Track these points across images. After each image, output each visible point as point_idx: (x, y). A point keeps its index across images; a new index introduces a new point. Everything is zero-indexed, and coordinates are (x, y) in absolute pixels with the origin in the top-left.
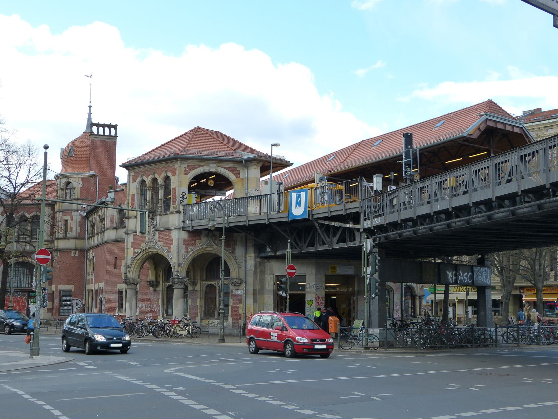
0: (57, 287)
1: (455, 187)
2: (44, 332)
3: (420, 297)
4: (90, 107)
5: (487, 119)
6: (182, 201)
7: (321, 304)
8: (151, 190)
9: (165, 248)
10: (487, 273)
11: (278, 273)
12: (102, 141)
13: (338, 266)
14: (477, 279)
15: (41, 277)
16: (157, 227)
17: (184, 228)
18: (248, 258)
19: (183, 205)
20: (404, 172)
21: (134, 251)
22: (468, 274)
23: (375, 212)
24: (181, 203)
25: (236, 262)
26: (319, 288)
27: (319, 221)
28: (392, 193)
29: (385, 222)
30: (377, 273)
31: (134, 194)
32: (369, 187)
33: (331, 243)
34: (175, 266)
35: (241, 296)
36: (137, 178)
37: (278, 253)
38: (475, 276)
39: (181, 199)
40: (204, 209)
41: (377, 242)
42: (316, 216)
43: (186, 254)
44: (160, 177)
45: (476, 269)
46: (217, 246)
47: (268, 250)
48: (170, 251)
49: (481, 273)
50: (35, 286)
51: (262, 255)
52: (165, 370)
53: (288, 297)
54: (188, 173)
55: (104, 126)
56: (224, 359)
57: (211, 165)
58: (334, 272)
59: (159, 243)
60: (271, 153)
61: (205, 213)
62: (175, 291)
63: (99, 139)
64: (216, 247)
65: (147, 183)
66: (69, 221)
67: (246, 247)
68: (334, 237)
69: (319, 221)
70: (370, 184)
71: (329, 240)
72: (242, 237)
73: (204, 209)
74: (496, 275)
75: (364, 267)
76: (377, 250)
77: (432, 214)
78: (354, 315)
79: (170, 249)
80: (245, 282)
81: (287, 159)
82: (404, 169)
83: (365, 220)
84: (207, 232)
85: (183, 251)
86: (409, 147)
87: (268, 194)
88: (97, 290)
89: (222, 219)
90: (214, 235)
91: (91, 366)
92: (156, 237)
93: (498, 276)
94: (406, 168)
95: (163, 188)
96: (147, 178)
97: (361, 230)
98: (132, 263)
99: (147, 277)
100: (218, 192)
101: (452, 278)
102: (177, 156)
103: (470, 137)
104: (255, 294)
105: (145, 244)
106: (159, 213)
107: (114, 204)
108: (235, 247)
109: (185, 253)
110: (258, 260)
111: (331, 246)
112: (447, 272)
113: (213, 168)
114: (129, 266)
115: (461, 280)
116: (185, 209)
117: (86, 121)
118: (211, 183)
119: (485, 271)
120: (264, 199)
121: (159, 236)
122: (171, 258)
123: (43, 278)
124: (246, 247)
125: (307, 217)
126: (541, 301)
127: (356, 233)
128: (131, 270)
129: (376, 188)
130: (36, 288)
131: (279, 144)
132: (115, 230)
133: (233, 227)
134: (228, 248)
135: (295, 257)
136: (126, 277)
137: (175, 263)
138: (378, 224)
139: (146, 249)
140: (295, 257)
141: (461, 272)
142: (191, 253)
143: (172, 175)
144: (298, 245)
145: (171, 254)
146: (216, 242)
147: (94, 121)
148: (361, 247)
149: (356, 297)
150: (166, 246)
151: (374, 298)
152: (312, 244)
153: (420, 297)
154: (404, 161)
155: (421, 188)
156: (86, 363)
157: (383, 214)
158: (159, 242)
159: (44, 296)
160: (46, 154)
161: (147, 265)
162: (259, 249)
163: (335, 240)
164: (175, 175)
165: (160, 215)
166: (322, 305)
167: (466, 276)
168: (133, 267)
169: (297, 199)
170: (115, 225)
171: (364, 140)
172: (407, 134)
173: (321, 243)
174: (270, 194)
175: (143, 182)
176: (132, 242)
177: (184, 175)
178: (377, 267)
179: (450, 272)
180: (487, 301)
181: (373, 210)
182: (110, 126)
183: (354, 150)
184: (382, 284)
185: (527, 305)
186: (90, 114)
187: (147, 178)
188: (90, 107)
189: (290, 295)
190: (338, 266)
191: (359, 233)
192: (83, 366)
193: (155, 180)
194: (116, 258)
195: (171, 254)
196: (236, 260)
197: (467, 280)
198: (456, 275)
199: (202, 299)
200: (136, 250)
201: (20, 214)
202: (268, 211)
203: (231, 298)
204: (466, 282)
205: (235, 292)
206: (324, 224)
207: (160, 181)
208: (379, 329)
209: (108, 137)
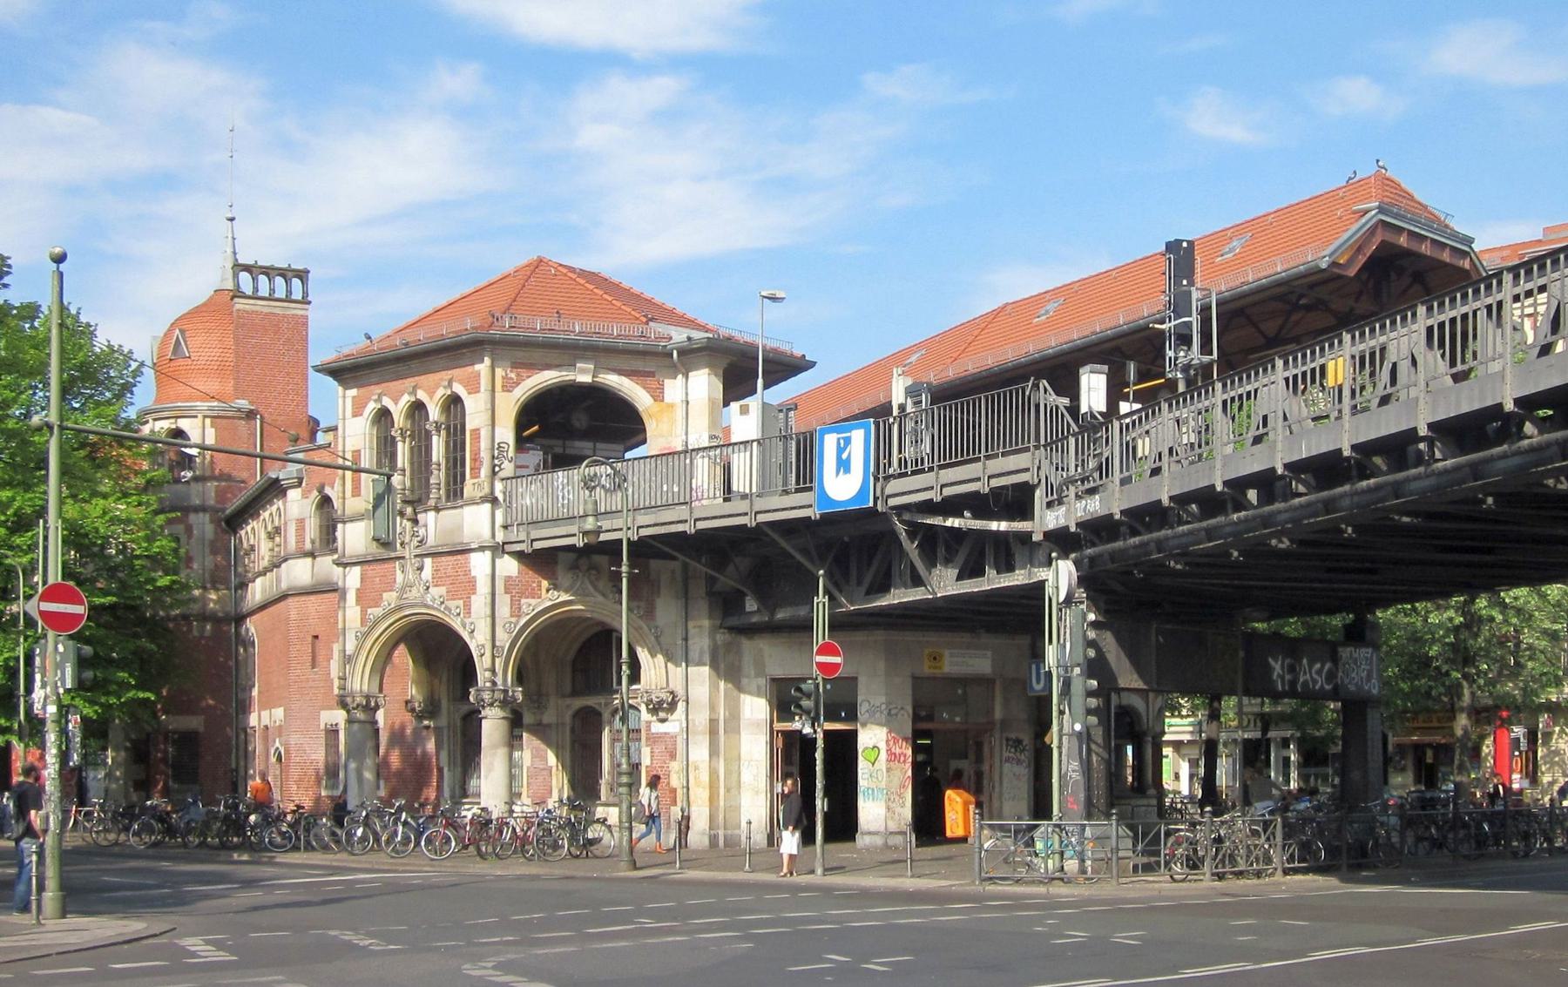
2: (1109, 838)
6: (500, 466)
7: (902, 759)
8: (407, 439)
9: (452, 604)
10: (1371, 663)
11: (779, 673)
12: (267, 314)
13: (947, 653)
14: (1346, 681)
15: (59, 672)
16: (428, 545)
18: (692, 631)
19: (503, 479)
20: (1170, 358)
21: (364, 612)
22: (1323, 666)
25: (659, 644)
26: (896, 715)
27: (907, 517)
28: (1134, 422)
31: (359, 451)
32: (1062, 408)
35: (674, 737)
36: (366, 404)
37: (781, 615)
38: (1340, 674)
40: (563, 489)
42: (893, 502)
43: (514, 620)
44: (431, 398)
45: (1345, 652)
46: (604, 595)
47: (751, 605)
48: (468, 612)
49: (1356, 664)
50: (42, 700)
52: (465, 966)
53: (820, 736)
54: (514, 388)
55: (269, 271)
56: (649, 923)
58: (936, 668)
59: (434, 591)
61: (566, 502)
62: (487, 726)
64: (600, 598)
65: (396, 417)
67: (687, 599)
69: (907, 517)
72: (673, 572)
73: (563, 489)
76: (1085, 595)
78: (993, 787)
79: (468, 607)
80: (684, 698)
81: (798, 352)
82: (1170, 349)
83: (1049, 505)
84: (572, 556)
85: (504, 610)
86: (1185, 282)
87: (753, 441)
88: (266, 727)
90: (593, 567)
91: (221, 953)
92: (427, 573)
95: (443, 433)
96: (396, 404)
98: (359, 649)
99: (405, 690)
100: (600, 445)
101: (1282, 678)
102: (480, 335)
103: (1336, 270)
104: (713, 731)
105: (394, 594)
106: (432, 503)
107: (304, 484)
108: (653, 600)
109: (512, 616)
110: (721, 637)
112: (1270, 660)
114: (350, 656)
115: (1305, 683)
116: (509, 489)
119: (1367, 658)
120: (742, 454)
121: (436, 571)
122: (473, 631)
123: (63, 674)
124: (687, 599)
125: (871, 504)
128: (356, 670)
129: (1090, 407)
130: (44, 707)
132: (309, 560)
133: (651, 541)
134: (635, 604)
135: (838, 625)
136: (342, 688)
137: (483, 646)
138: (1095, 516)
139: (400, 608)
141: (1305, 661)
142: (528, 617)
143: (469, 393)
145: (470, 620)
146: (601, 584)
150: (454, 599)
154: (1169, 325)
156: (208, 942)
158: (436, 586)
161: (402, 655)
162: (726, 606)
164: (475, 393)
165: (437, 509)
166: (904, 761)
167: (1319, 672)
168: (362, 658)
169: (840, 451)
170: (308, 546)
171: (1007, 304)
174: (758, 441)
175: (383, 415)
176: (358, 590)
177: (503, 391)
179: (1276, 662)
180: (1369, 743)
182: (285, 273)
183: (983, 330)
185: (1397, 758)
187: (396, 401)
189: (827, 733)
190: (947, 653)
192: (194, 955)
193: (418, 408)
194: (316, 637)
195: (470, 620)
197: (1321, 683)
198: (1292, 669)
199: (563, 747)
200: (369, 611)
203: (647, 746)
204: (1317, 687)
205: (658, 728)
207: (434, 413)
209: (286, 304)
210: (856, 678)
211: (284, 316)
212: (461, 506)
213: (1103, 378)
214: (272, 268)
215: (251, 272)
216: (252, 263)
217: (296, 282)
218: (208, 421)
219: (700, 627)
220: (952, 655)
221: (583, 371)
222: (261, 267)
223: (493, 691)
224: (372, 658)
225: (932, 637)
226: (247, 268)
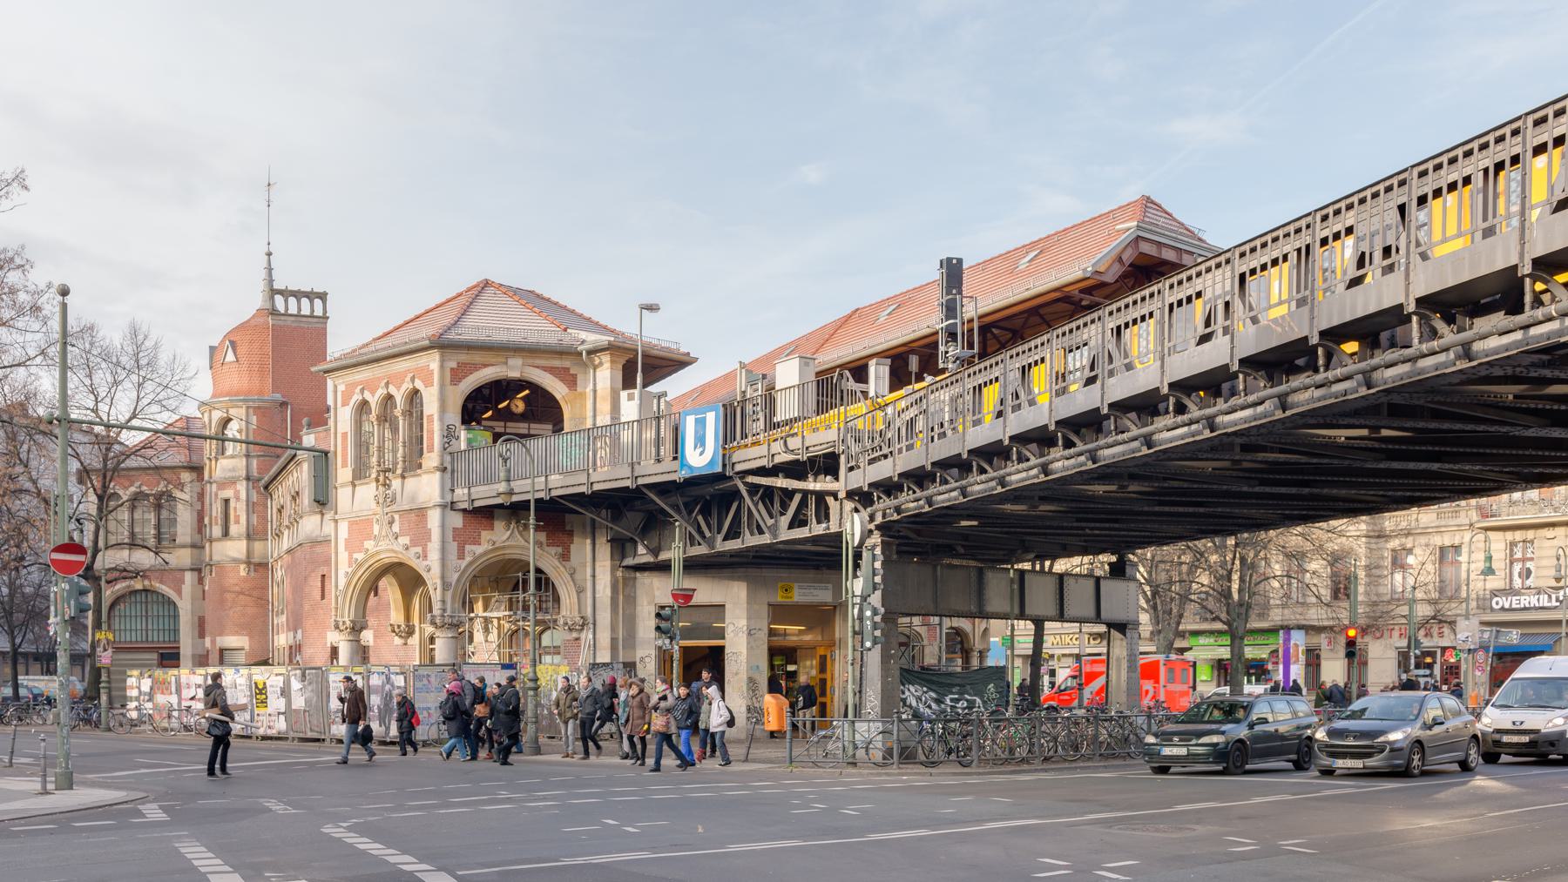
0: (213, 642)
1: (1063, 375)
3: (980, 652)
4: (269, 254)
5: (1138, 237)
12: (295, 328)
17: (452, 505)
23: (873, 449)
24: (445, 449)
25: (573, 580)
27: (751, 479)
29: (894, 471)
30: (878, 593)
33: (774, 530)
34: (435, 589)
39: (446, 440)
41: (879, 519)
42: (739, 468)
47: (641, 550)
51: (629, 561)
55: (298, 295)
57: (511, 362)
58: (787, 597)
60: (638, 333)
63: (289, 323)
65: (373, 406)
66: (232, 504)
68: (782, 514)
69: (751, 479)
70: (862, 386)
71: (770, 522)
74: (1143, 609)
75: (847, 579)
76: (879, 540)
77: (1006, 442)
81: (683, 350)
89: (529, 481)
93: (1147, 611)
94: (947, 342)
97: (842, 495)
111: (775, 538)
113: (513, 369)
117: (260, 286)
118: (519, 406)
126: (1240, 658)
127: (830, 500)
131: (657, 305)
140: (693, 566)
144: (704, 537)
147: (276, 286)
148: (839, 535)
149: (837, 652)
151: (869, 649)
152: (733, 533)
153: (980, 652)
155: (980, 385)
157: (891, 452)
159: (1156, 735)
160: (64, 306)
163: (785, 521)
172: (949, 260)
173: (756, 531)
174: (638, 421)
178: (878, 579)
181: (868, 445)
182: (310, 296)
184: (890, 618)
186: (270, 270)
188: (269, 254)
190: (796, 585)
191: (838, 502)
196: (572, 575)
201: (133, 489)
202: (635, 460)
206: (760, 486)
208: (883, 722)
209: (310, 319)
210: (724, 606)
211: (308, 328)
212: (419, 475)
213: (887, 369)
214: (312, 292)
215: (295, 296)
216: (284, 288)
217: (318, 302)
218: (251, 411)
219: (604, 566)
220: (800, 588)
221: (512, 368)
222: (291, 291)
223: (1415, 601)
224: (357, 591)
225: (784, 573)
226: (280, 292)
